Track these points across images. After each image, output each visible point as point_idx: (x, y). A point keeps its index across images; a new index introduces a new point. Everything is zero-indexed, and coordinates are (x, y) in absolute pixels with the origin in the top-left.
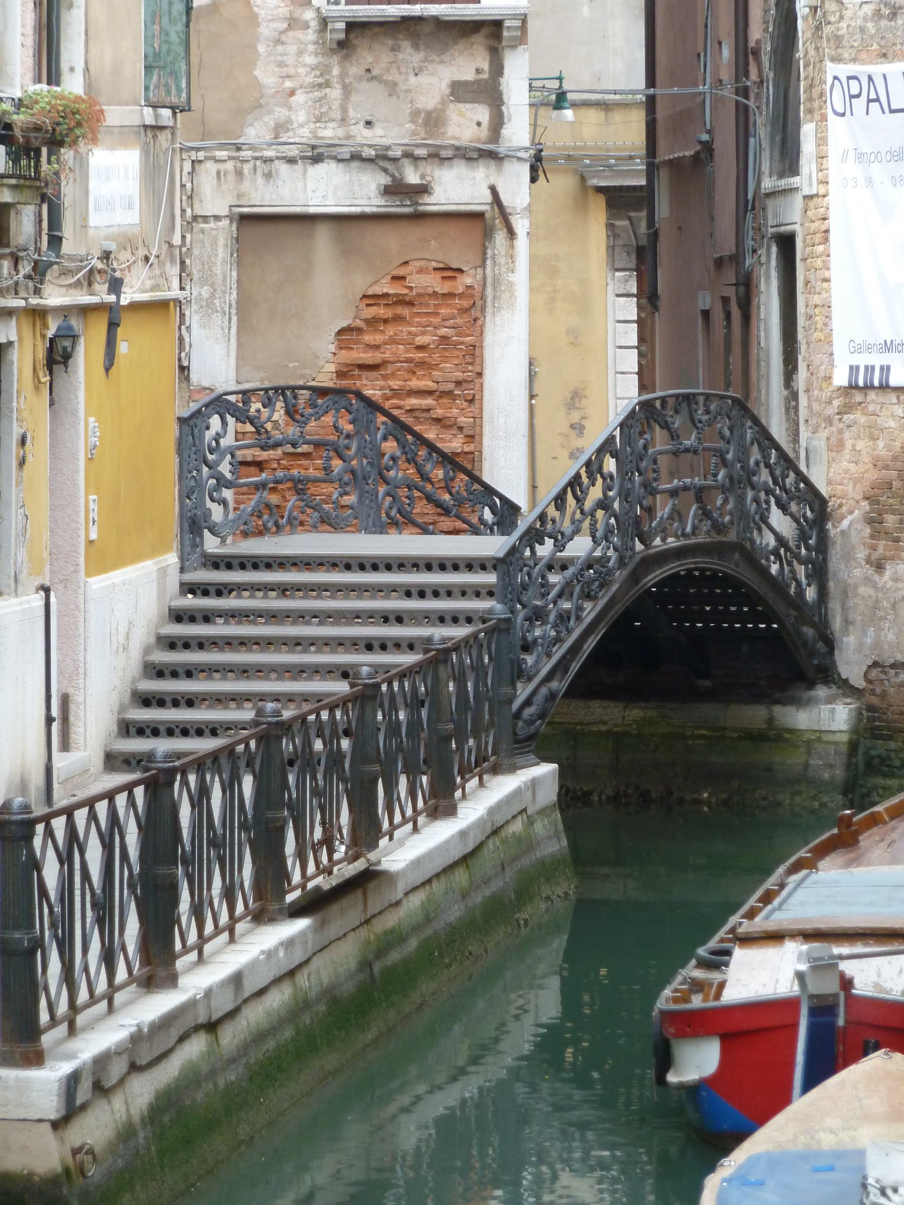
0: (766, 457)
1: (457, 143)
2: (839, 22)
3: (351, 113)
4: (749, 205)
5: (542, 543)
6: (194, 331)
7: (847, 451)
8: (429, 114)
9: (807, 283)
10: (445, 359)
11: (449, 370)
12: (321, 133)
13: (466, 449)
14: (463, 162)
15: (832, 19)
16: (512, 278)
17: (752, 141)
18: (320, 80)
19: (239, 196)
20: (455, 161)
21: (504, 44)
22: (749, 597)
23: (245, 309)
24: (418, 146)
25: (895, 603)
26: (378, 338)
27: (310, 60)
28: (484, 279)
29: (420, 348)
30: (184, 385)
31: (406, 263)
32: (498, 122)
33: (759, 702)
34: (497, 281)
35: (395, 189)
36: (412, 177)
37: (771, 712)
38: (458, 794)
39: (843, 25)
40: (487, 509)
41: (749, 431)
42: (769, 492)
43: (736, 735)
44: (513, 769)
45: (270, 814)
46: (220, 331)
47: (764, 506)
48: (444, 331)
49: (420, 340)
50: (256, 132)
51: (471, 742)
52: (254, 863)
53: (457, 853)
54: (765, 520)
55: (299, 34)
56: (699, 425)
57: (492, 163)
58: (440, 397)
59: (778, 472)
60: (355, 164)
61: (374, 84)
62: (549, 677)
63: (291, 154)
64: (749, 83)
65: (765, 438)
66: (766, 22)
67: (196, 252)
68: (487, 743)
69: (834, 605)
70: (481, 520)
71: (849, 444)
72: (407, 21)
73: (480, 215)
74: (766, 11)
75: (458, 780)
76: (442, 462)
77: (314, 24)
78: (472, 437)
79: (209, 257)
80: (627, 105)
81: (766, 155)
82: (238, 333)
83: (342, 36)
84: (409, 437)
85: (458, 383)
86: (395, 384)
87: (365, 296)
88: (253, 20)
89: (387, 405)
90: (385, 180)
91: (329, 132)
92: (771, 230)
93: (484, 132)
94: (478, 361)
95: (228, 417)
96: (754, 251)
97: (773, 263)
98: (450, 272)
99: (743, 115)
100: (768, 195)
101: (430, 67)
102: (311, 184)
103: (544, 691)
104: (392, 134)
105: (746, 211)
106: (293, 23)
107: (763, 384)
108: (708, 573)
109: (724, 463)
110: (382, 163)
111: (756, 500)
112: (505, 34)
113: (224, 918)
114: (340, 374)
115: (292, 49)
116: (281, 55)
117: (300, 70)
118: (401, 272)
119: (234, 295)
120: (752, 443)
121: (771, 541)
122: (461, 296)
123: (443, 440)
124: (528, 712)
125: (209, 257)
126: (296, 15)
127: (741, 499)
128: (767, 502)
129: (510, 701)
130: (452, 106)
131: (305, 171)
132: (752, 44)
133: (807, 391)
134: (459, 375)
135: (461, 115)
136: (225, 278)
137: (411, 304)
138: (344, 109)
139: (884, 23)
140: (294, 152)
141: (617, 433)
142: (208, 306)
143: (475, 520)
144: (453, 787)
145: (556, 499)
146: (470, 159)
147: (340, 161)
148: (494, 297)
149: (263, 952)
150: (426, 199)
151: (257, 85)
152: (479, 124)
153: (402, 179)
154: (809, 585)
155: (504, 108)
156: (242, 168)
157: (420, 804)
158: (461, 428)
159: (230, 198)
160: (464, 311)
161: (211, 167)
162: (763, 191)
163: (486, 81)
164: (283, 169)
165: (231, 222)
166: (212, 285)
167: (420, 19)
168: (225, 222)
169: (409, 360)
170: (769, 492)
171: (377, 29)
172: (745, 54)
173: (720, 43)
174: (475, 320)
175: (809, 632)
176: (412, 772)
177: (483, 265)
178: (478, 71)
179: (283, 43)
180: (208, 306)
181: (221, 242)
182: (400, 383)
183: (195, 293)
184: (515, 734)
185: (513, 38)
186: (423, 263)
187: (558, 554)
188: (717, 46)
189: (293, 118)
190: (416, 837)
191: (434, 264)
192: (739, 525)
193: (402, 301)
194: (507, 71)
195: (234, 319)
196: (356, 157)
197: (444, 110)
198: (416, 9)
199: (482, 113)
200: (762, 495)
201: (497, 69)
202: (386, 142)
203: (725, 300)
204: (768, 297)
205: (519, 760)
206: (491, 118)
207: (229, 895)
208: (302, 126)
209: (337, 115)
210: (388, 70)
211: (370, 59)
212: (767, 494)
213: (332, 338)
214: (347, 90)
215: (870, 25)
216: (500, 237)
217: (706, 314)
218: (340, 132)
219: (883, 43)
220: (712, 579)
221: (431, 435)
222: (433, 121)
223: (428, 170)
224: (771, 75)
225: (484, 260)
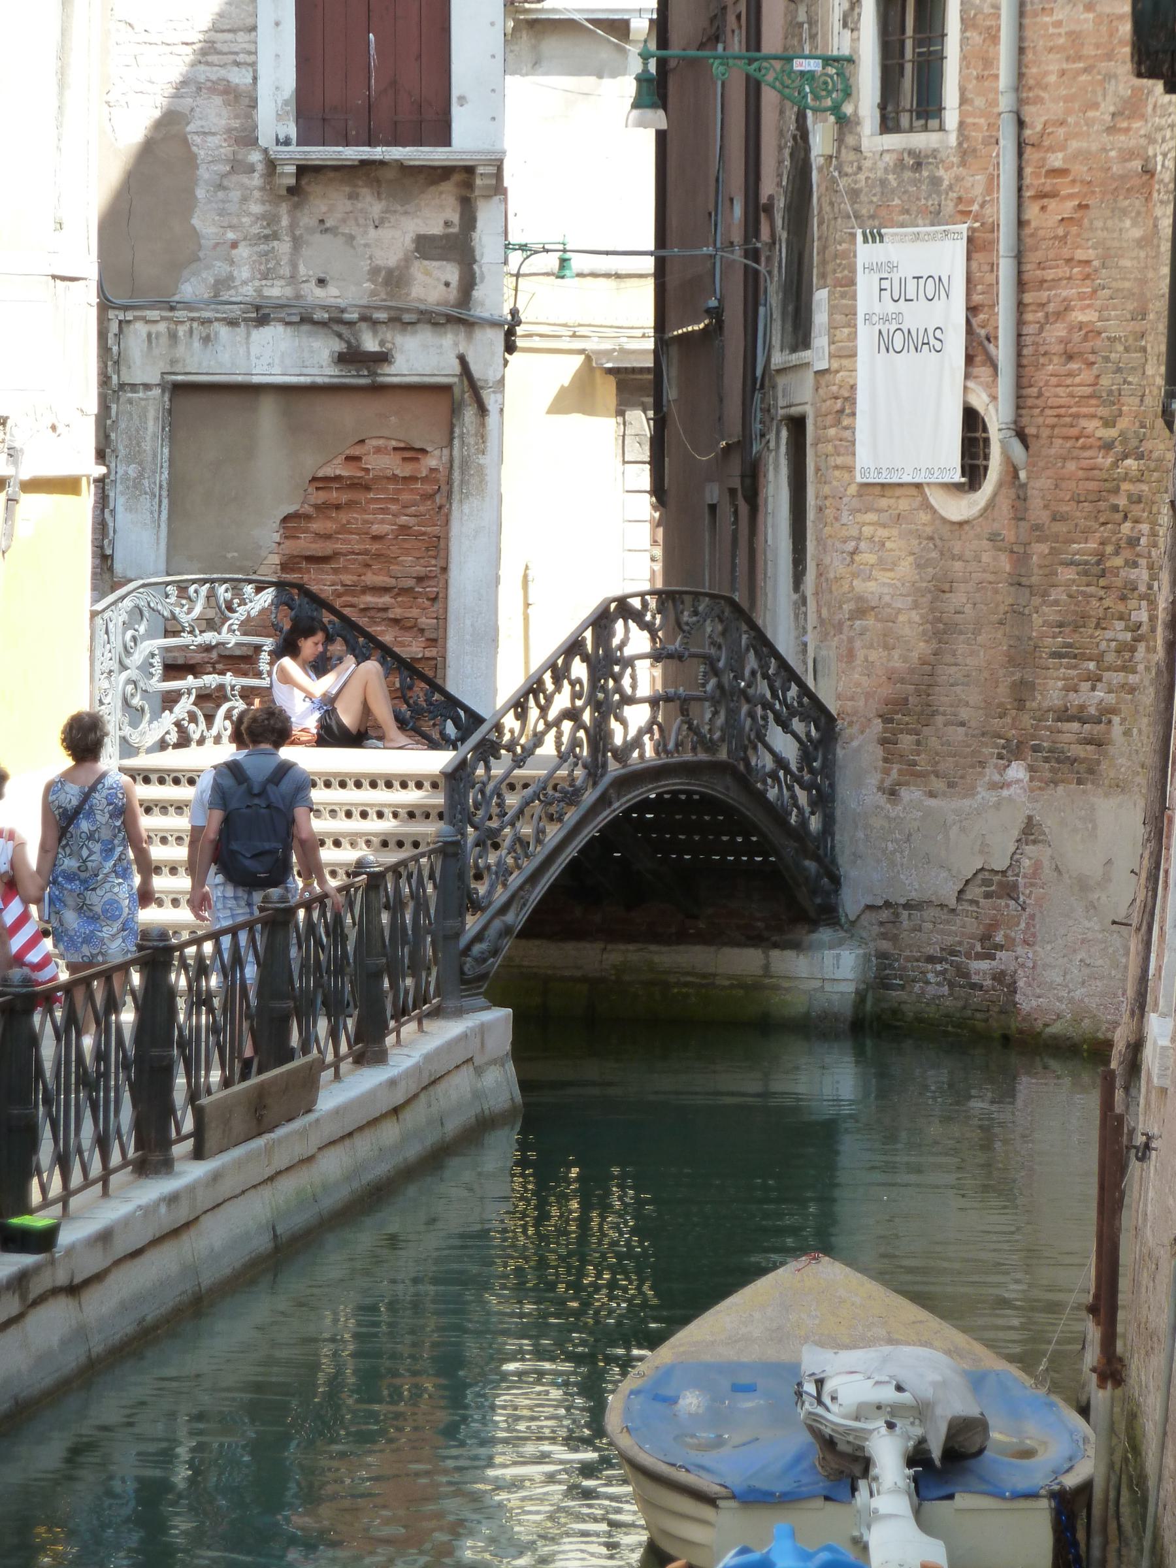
0: (764, 667)
1: (422, 307)
2: (856, 174)
3: (302, 270)
4: (757, 383)
5: (498, 757)
6: (119, 516)
7: (858, 662)
8: (390, 272)
9: (818, 470)
10: (407, 552)
11: (409, 565)
12: (267, 292)
13: (428, 654)
14: (428, 327)
15: (849, 170)
16: (482, 460)
17: (762, 310)
18: (267, 231)
19: (173, 362)
20: (419, 326)
21: (477, 193)
22: (738, 823)
23: (178, 494)
24: (378, 308)
25: (910, 835)
26: (328, 526)
27: (256, 208)
28: (451, 461)
29: (376, 538)
30: (107, 576)
31: (362, 441)
32: (468, 283)
33: (755, 946)
34: (465, 464)
35: (351, 357)
36: (370, 344)
37: (767, 957)
38: (390, 1040)
39: (861, 177)
40: (449, 723)
41: (744, 637)
42: (767, 706)
43: (727, 983)
44: (459, 1013)
45: (155, 1052)
46: (148, 515)
47: (761, 722)
48: (404, 519)
49: (376, 529)
50: (191, 289)
51: (409, 981)
52: (134, 1106)
53: (384, 1106)
54: (761, 738)
55: (244, 179)
56: (686, 628)
57: (462, 329)
58: (398, 594)
59: (777, 684)
60: (305, 328)
61: (328, 237)
62: (504, 909)
63: (232, 315)
64: (759, 245)
65: (764, 645)
66: (780, 175)
67: (122, 425)
68: (428, 983)
69: (842, 837)
70: (442, 734)
71: (860, 654)
72: (365, 164)
73: (446, 389)
74: (780, 162)
75: (392, 1024)
76: (398, 668)
77: (260, 167)
78: (435, 640)
79: (137, 431)
81: (777, 328)
82: (169, 518)
83: (292, 181)
84: (361, 640)
85: (420, 579)
86: (348, 579)
87: (314, 479)
88: (191, 161)
89: (337, 604)
90: (339, 346)
91: (276, 291)
92: (781, 412)
93: (453, 294)
94: (442, 554)
96: (763, 435)
97: (783, 449)
98: (411, 453)
99: (753, 281)
100: (778, 371)
101: (393, 219)
102: (254, 350)
103: (497, 924)
104: (348, 292)
105: (754, 390)
106: (238, 166)
107: (770, 583)
108: (696, 797)
109: (716, 673)
110: (336, 327)
111: (751, 715)
112: (478, 182)
113: (96, 1168)
114: (284, 567)
115: (235, 195)
116: (223, 202)
117: (244, 220)
118: (357, 451)
119: (166, 475)
120: (748, 650)
121: (769, 763)
122: (425, 480)
123: (402, 644)
124: (477, 948)
125: (137, 431)
126: (240, 157)
127: (732, 713)
128: (765, 718)
129: (457, 935)
130: (417, 263)
131: (248, 335)
132: (764, 200)
133: (816, 594)
134: (419, 570)
135: (428, 273)
136: (155, 456)
137: (367, 488)
138: (294, 266)
139: (908, 174)
140: (235, 311)
141: (588, 634)
142: (135, 487)
143: (436, 736)
144: (383, 1031)
146: (436, 324)
147: (288, 324)
148: (462, 482)
149: (140, 1207)
150: (387, 369)
151: (195, 234)
152: (447, 284)
153: (359, 346)
154: (813, 813)
155: (475, 267)
156: (176, 331)
157: (344, 1048)
158: (422, 631)
159: (161, 364)
160: (431, 497)
161: (141, 328)
162: (773, 367)
163: (456, 236)
164: (223, 331)
165: (163, 391)
166: (140, 464)
167: (382, 163)
168: (157, 392)
169: (366, 552)
170: (767, 706)
171: (332, 174)
172: (756, 209)
173: (732, 200)
174: (440, 508)
175: (811, 865)
176: (335, 1009)
177: (450, 444)
178: (447, 224)
179: (225, 188)
180: (135, 487)
181: (151, 414)
182: (355, 578)
183: (121, 472)
184: (462, 973)
185: (487, 187)
186: (381, 442)
187: (517, 772)
188: (728, 203)
189: (235, 273)
190: (336, 1085)
191: (394, 443)
192: (730, 743)
193: (356, 485)
194: (480, 224)
195: (165, 502)
196: (306, 320)
197: (407, 267)
198: (378, 152)
199: (451, 272)
200: (759, 711)
201: (469, 221)
202: (342, 303)
203: (732, 492)
204: (777, 488)
205: (467, 1002)
206: (461, 279)
207: (102, 1143)
208: (245, 283)
209: (286, 271)
210: (344, 221)
211: (324, 209)
212: (764, 708)
213: (276, 525)
214: (297, 243)
215: (891, 177)
216: (469, 413)
217: (713, 508)
218: (289, 292)
219: (905, 198)
220: (708, 803)
221: (387, 638)
222: (394, 279)
223: (389, 336)
224: (784, 235)
225: (452, 439)
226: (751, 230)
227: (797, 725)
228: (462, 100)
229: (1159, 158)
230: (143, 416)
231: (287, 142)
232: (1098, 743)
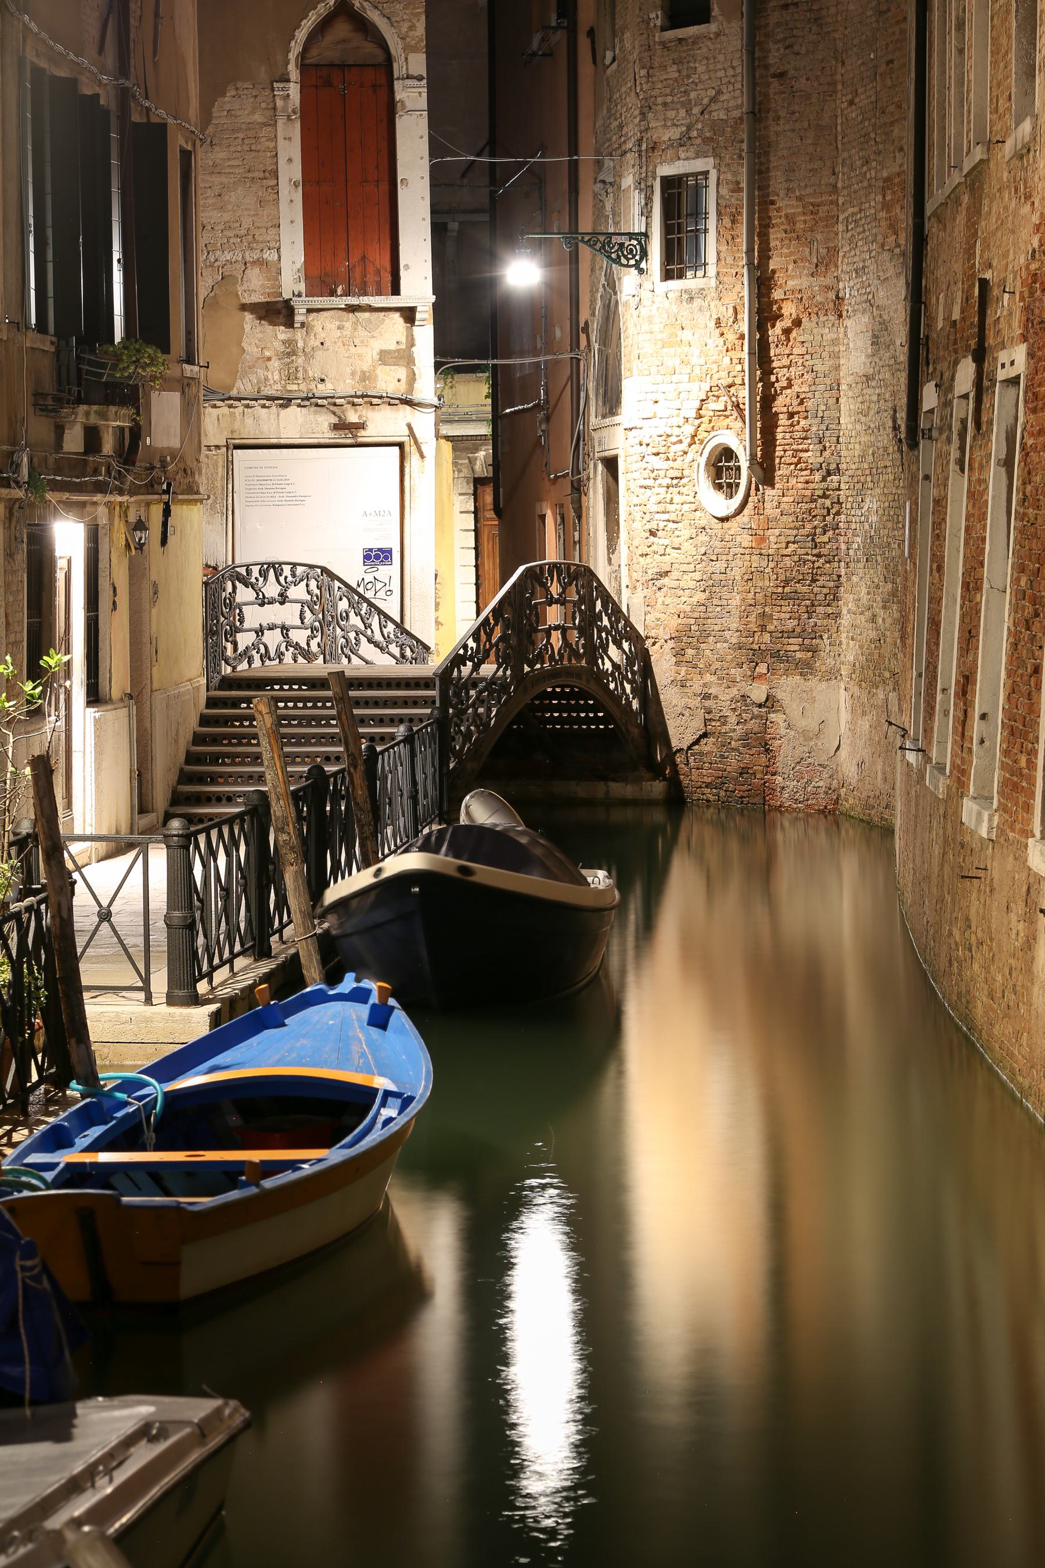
5: (465, 665)
17: (582, 394)
18: (288, 350)
19: (232, 432)
32: (412, 378)
35: (341, 426)
36: (352, 417)
80: (607, 318)
90: (334, 420)
95: (237, 583)
97: (599, 478)
121: (608, 665)
128: (607, 639)
130: (380, 368)
145: (473, 635)
150: (362, 433)
154: (633, 698)
199: (402, 373)
206: (407, 376)
224: (597, 346)
226: (574, 345)
227: (626, 645)
228: (407, 267)
229: (847, 290)
230: (216, 466)
231: (300, 295)
232: (814, 651)
